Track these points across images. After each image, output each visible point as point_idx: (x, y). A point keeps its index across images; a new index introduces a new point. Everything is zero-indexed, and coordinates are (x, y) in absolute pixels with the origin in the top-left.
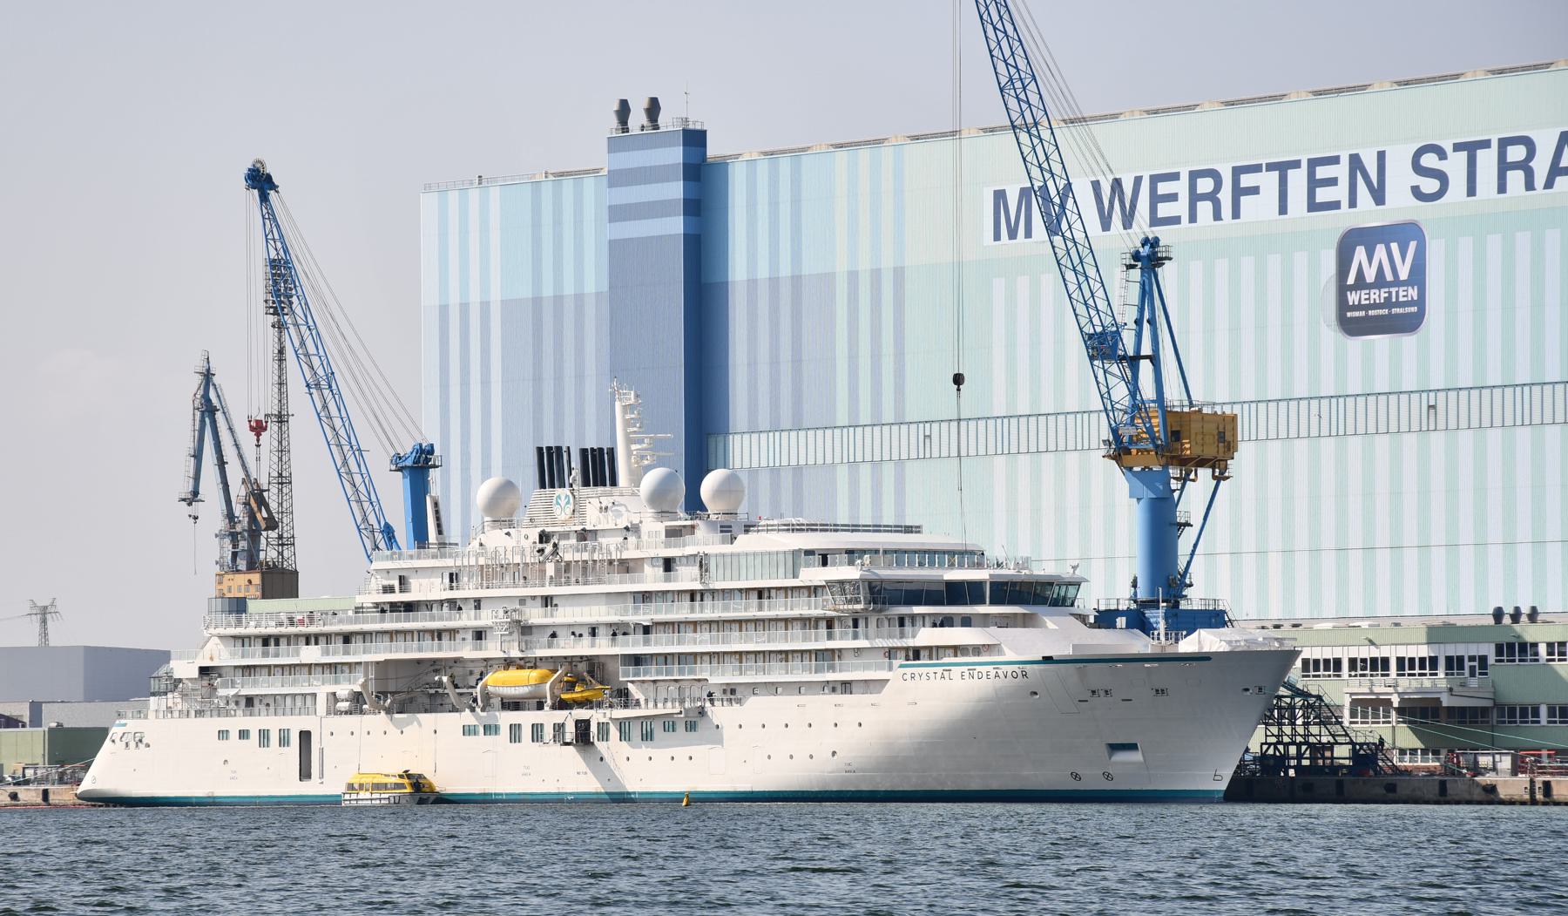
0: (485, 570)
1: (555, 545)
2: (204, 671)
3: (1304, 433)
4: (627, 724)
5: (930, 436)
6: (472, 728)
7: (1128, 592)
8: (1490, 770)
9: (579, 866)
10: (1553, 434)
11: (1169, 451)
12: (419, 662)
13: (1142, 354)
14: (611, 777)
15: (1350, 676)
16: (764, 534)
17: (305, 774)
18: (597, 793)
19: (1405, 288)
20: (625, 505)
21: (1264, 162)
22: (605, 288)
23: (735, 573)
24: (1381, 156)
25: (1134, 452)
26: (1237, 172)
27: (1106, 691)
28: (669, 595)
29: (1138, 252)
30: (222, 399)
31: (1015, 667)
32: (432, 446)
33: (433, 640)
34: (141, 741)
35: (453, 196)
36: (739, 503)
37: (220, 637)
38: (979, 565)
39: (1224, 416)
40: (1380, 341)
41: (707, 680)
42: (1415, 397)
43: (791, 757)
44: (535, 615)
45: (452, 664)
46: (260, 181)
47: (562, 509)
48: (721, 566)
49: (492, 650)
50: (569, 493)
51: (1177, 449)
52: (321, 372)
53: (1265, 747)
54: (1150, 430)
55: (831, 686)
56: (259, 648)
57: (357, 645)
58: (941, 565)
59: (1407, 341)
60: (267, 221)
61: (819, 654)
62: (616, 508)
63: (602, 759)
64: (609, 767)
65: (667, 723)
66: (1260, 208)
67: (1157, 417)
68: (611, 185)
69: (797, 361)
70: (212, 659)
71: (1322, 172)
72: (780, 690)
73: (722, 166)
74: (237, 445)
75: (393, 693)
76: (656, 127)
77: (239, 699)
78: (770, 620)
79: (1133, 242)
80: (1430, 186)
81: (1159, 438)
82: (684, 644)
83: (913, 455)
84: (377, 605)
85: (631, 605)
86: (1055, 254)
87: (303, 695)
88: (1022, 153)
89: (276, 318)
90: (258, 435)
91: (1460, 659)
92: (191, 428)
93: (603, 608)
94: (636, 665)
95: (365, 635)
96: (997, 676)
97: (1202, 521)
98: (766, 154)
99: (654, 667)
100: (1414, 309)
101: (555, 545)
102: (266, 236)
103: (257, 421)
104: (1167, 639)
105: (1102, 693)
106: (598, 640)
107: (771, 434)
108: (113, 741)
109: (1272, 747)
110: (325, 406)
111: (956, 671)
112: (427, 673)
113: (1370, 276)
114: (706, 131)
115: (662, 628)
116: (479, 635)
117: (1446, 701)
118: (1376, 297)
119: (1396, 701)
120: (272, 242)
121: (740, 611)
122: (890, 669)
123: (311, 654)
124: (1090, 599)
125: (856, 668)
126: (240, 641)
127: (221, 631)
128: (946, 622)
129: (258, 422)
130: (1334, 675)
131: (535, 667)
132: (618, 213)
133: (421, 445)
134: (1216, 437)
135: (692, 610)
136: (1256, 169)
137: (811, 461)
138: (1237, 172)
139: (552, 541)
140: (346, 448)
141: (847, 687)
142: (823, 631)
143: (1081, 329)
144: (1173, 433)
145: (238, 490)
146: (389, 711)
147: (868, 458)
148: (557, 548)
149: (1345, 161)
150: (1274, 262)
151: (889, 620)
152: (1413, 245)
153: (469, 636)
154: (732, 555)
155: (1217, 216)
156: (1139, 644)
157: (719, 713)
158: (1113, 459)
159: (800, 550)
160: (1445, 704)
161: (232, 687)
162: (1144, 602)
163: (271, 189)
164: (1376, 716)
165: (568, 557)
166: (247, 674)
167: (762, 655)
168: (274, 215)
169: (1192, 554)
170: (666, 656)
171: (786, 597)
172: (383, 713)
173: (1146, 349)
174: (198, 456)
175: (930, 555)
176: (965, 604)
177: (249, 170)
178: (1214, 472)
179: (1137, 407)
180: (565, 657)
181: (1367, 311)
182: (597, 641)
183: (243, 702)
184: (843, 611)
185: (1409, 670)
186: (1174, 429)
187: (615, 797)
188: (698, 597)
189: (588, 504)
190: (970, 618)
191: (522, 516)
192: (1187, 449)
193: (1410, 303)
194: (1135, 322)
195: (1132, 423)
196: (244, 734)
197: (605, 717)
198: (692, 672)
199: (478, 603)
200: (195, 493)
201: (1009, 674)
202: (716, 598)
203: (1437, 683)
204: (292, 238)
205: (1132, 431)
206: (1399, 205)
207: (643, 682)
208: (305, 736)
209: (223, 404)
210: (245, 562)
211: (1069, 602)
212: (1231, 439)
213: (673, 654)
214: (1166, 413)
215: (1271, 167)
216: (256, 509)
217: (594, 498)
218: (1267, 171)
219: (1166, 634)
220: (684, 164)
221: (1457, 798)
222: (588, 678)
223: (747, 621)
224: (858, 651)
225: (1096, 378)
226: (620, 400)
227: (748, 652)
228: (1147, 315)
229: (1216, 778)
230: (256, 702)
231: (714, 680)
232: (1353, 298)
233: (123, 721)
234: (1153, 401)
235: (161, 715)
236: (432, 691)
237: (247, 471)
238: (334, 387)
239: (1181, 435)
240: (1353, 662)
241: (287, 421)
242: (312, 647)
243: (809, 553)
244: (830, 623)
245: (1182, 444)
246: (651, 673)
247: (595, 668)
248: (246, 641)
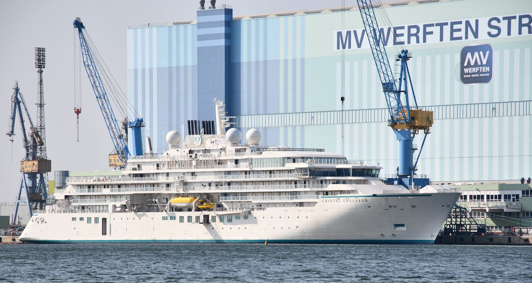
1: (196, 155)
2: (66, 197)
3: (448, 117)
5: (313, 117)
7: (396, 172)
8: (526, 234)
9: (398, 263)
10: (527, 118)
11: (411, 124)
12: (145, 194)
13: (402, 90)
14: (216, 235)
15: (470, 201)
16: (272, 151)
17: (104, 233)
18: (211, 240)
19: (485, 67)
21: (435, 23)
22: (196, 63)
23: (262, 165)
24: (477, 21)
25: (398, 124)
26: (425, 26)
27: (395, 206)
28: (237, 172)
31: (363, 198)
32: (142, 119)
33: (151, 187)
34: (43, 221)
35: (139, 31)
36: (259, 140)
37: (72, 185)
40: (476, 85)
41: (251, 202)
42: (488, 105)
43: (282, 228)
44: (189, 179)
45: (157, 195)
46: (79, 25)
48: (257, 162)
49: (173, 190)
50: (200, 137)
51: (413, 123)
53: (446, 226)
54: (404, 117)
55: (296, 204)
58: (334, 162)
59: (485, 86)
60: (81, 39)
61: (292, 193)
62: (217, 142)
63: (213, 228)
66: (433, 39)
67: (406, 112)
68: (198, 28)
69: (265, 90)
70: (69, 193)
71: (456, 27)
72: (277, 205)
73: (239, 21)
74: (28, 115)
75: (136, 205)
76: (214, 8)
79: (398, 51)
80: (494, 32)
81: (407, 119)
82: (243, 189)
83: (307, 124)
84: (130, 175)
86: (374, 56)
88: (363, 21)
89: (39, 69)
90: (78, 114)
91: (509, 196)
93: (214, 177)
95: (126, 185)
97: (421, 148)
98: (254, 17)
100: (488, 75)
101: (196, 155)
102: (81, 44)
103: (78, 110)
104: (414, 189)
105: (393, 207)
106: (211, 187)
107: (256, 116)
108: (33, 221)
109: (449, 225)
110: (103, 105)
111: (342, 199)
113: (472, 63)
114: (232, 9)
115: (235, 183)
116: (168, 185)
117: (505, 210)
118: (475, 70)
119: (487, 210)
120: (83, 47)
121: (263, 178)
122: (318, 198)
123: (106, 191)
124: (383, 175)
126: (80, 187)
127: (73, 183)
128: (338, 182)
129: (78, 110)
131: (187, 196)
132: (200, 38)
136: (432, 25)
137: (270, 125)
138: (425, 26)
141: (301, 204)
142: (293, 185)
143: (382, 82)
145: (29, 131)
146: (135, 211)
150: (438, 58)
151: (317, 181)
152: (488, 52)
153: (164, 186)
154: (261, 159)
155: (418, 41)
157: (256, 213)
158: (391, 126)
159: (285, 157)
160: (505, 211)
161: (77, 202)
164: (479, 214)
165: (201, 158)
166: (82, 198)
167: (271, 193)
168: (84, 37)
170: (236, 193)
171: (280, 173)
173: (403, 89)
174: (13, 119)
175: (329, 159)
176: (343, 176)
177: (75, 21)
178: (425, 131)
179: (400, 107)
180: (199, 193)
183: (81, 208)
184: (301, 178)
187: (218, 241)
188: (248, 173)
190: (345, 181)
192: (417, 123)
193: (487, 72)
194: (399, 79)
198: (246, 199)
199: (168, 174)
200: (12, 132)
201: (361, 200)
202: (254, 173)
203: (502, 204)
204: (90, 45)
205: (398, 117)
206: (483, 38)
207: (228, 202)
208: (104, 220)
210: (31, 157)
211: (376, 176)
212: (431, 120)
214: (410, 111)
215: (437, 25)
216: (36, 138)
219: (414, 187)
220: (225, 21)
221: (514, 243)
222: (208, 200)
223: (266, 181)
224: (306, 192)
226: (217, 104)
227: (266, 192)
230: (86, 208)
231: (254, 201)
232: (466, 70)
233: (37, 214)
234: (405, 107)
237: (32, 124)
238: (106, 98)
240: (471, 196)
242: (106, 189)
243: (288, 158)
244: (296, 182)
245: (415, 122)
246: (231, 199)
248: (82, 186)
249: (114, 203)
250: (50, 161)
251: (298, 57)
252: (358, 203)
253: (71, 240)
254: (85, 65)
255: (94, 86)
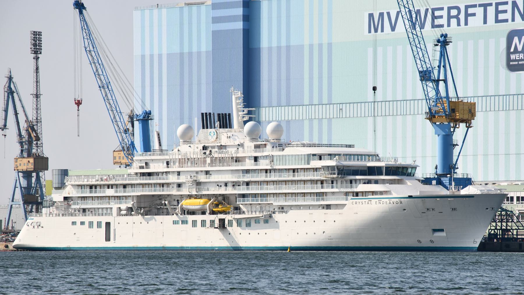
0: (181, 160)
1: (210, 151)
2: (66, 198)
3: (492, 109)
4: (258, 220)
5: (342, 109)
6: (177, 222)
11: (451, 116)
14: (233, 241)
15: (517, 203)
17: (108, 239)
18: (227, 247)
20: (237, 136)
21: (478, 3)
23: (284, 163)
25: (437, 116)
26: (467, 7)
27: (433, 209)
29: (439, 39)
30: (16, 88)
31: (397, 200)
33: (160, 187)
34: (40, 225)
36: (281, 135)
37: (72, 185)
38: (379, 160)
39: (471, 103)
41: (272, 204)
43: (307, 234)
44: (202, 178)
45: (167, 196)
47: (212, 137)
48: (278, 160)
49: (185, 191)
50: (215, 131)
52: (104, 82)
53: (490, 231)
54: (444, 109)
55: (322, 206)
56: (88, 190)
57: (128, 189)
63: (230, 234)
64: (233, 237)
65: (256, 220)
66: (476, 22)
67: (446, 103)
69: (288, 79)
70: (69, 194)
71: (501, 8)
75: (144, 208)
77: (80, 210)
78: (298, 181)
81: (447, 112)
84: (136, 174)
85: (242, 174)
86: (409, 40)
87: (106, 208)
90: (78, 106)
92: (3, 99)
93: (230, 176)
94: (243, 198)
95: (132, 185)
96: (390, 203)
99: (250, 199)
101: (210, 151)
103: (78, 101)
104: (455, 189)
105: (431, 210)
108: (28, 225)
109: (493, 231)
110: (106, 95)
112: (156, 200)
115: (254, 183)
116: (179, 185)
120: (84, 30)
121: (286, 177)
122: (347, 200)
123: (110, 192)
124: (420, 174)
125: (334, 199)
126: (81, 187)
127: (73, 183)
128: (369, 182)
129: (78, 101)
130: (511, 203)
131: (201, 198)
132: (216, 20)
133: (146, 111)
134: (468, 111)
135: (266, 176)
136: (475, 6)
138: (467, 7)
139: (209, 150)
140: (115, 112)
141: (328, 207)
142: (319, 185)
143: (418, 69)
144: (452, 109)
145: (23, 125)
146: (142, 215)
147: (317, 117)
148: (211, 152)
149: (510, 4)
151: (346, 181)
153: (175, 186)
154: (283, 156)
155: (459, 24)
156: (442, 191)
157: (277, 216)
158: (428, 119)
159: (310, 154)
161: (77, 205)
162: (441, 174)
163: (83, 9)
165: (216, 155)
166: (83, 200)
168: (85, 20)
169: (459, 155)
172: (140, 215)
173: (442, 77)
174: (6, 111)
175: (360, 156)
176: (375, 175)
178: (466, 125)
180: (214, 195)
181: (518, 62)
182: (228, 189)
183: (82, 211)
184: (328, 178)
185: (521, 201)
186: (452, 108)
188: (269, 171)
189: (222, 135)
191: (196, 139)
192: (458, 116)
194: (438, 67)
195: (436, 105)
196: (203, 223)
197: (232, 217)
198: (266, 200)
199: (179, 173)
200: (5, 126)
201: (395, 202)
207: (246, 204)
208: (108, 224)
209: (17, 90)
211: (412, 175)
213: (258, 194)
214: (450, 102)
215: (480, 5)
217: (224, 133)
218: (477, 5)
219: (455, 187)
222: (224, 202)
223: (288, 181)
224: (333, 193)
225: (423, 88)
226: (235, 95)
228: (442, 64)
229: (475, 242)
230: (87, 211)
232: (513, 57)
233: (32, 218)
235: (48, 215)
236: (159, 207)
237: (27, 117)
239: (455, 110)
240: (518, 198)
241: (40, 97)
242: (110, 190)
243: (314, 155)
244: (322, 182)
245: (456, 114)
246: (249, 200)
247: (225, 197)
248: (83, 187)
249: (119, 206)
250: (47, 158)
251: (325, 41)
252: (391, 206)
253: (71, 247)
254: (86, 51)
255: (97, 74)
